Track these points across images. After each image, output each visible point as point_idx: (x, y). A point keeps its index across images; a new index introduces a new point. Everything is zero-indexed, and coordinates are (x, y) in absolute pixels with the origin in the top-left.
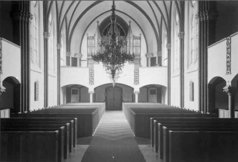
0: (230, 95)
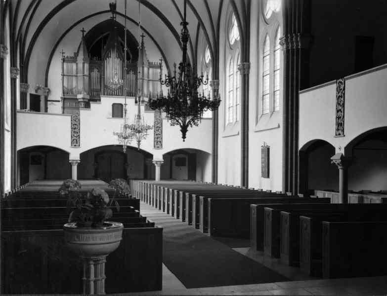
0: (341, 169)
